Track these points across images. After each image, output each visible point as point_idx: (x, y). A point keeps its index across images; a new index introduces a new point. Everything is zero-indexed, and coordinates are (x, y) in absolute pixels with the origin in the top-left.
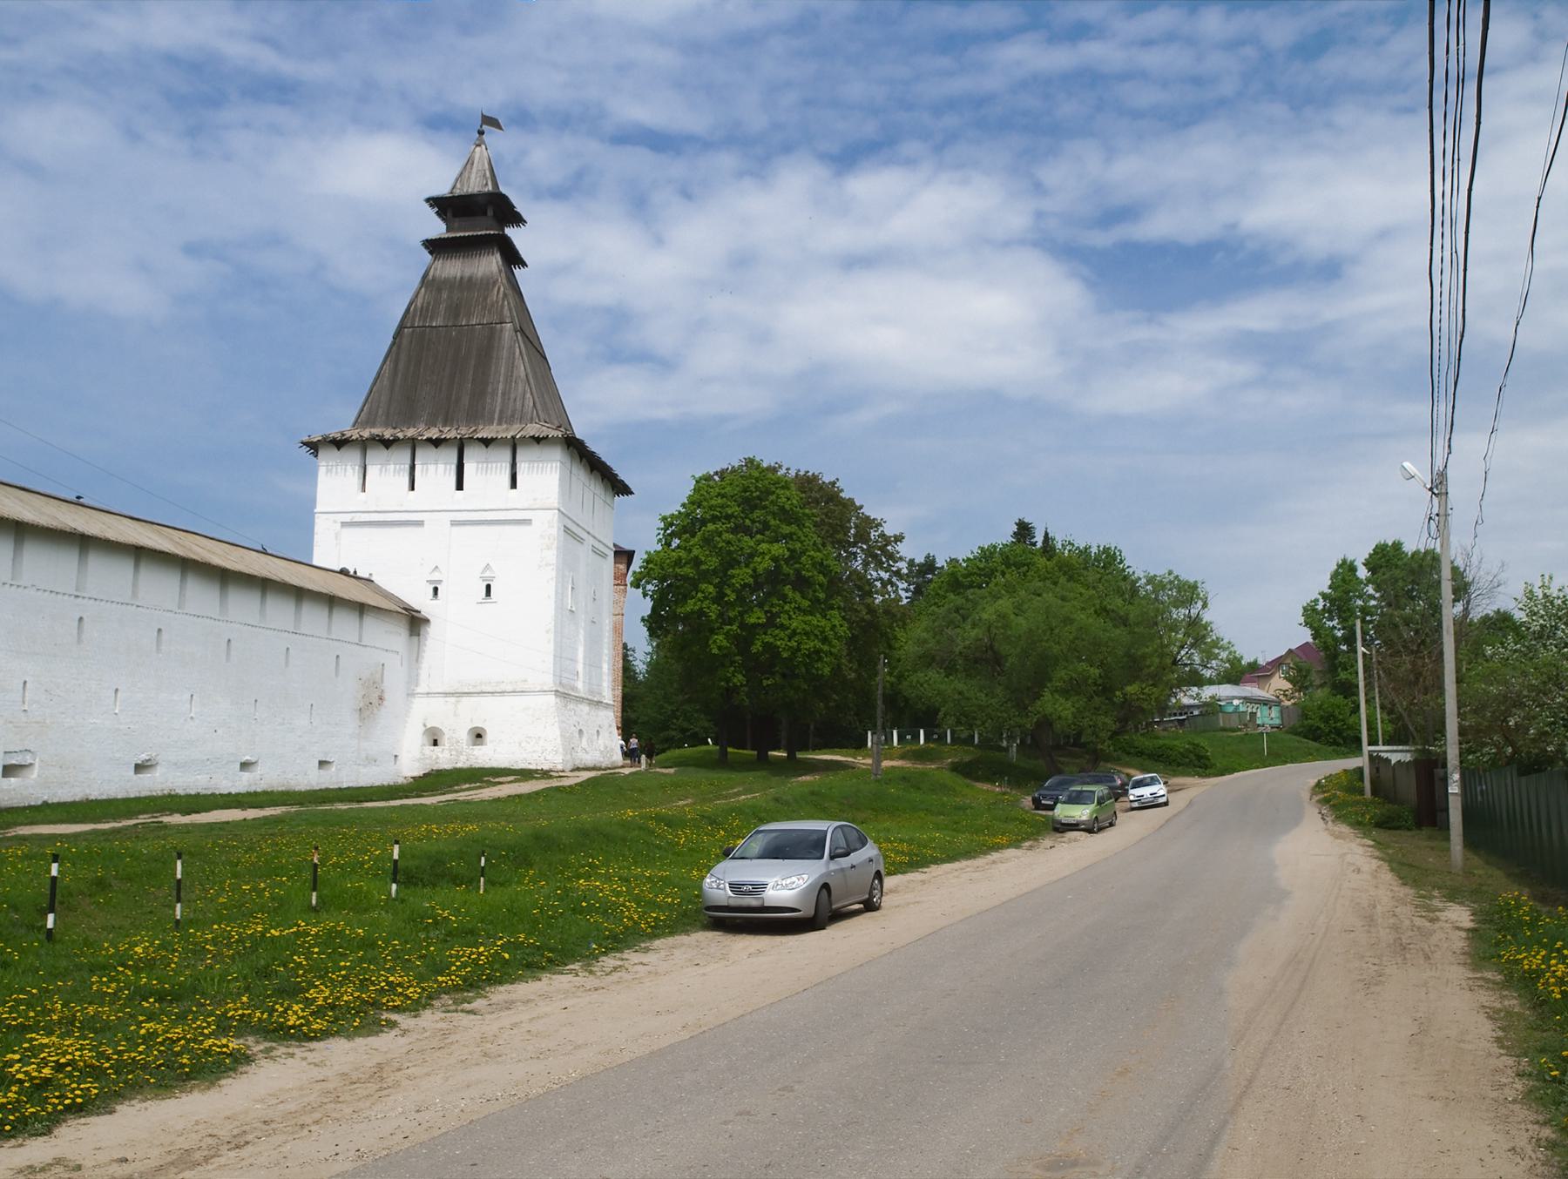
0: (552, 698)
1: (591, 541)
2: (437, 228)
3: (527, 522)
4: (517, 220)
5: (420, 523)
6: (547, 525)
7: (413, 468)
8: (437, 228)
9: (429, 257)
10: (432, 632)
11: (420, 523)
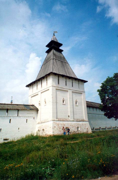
0: (52, 122)
1: (71, 91)
2: (48, 48)
3: (48, 90)
4: (61, 45)
5: (38, 94)
6: (51, 89)
7: (37, 85)
8: (48, 48)
9: (47, 54)
10: (39, 112)
11: (38, 94)
